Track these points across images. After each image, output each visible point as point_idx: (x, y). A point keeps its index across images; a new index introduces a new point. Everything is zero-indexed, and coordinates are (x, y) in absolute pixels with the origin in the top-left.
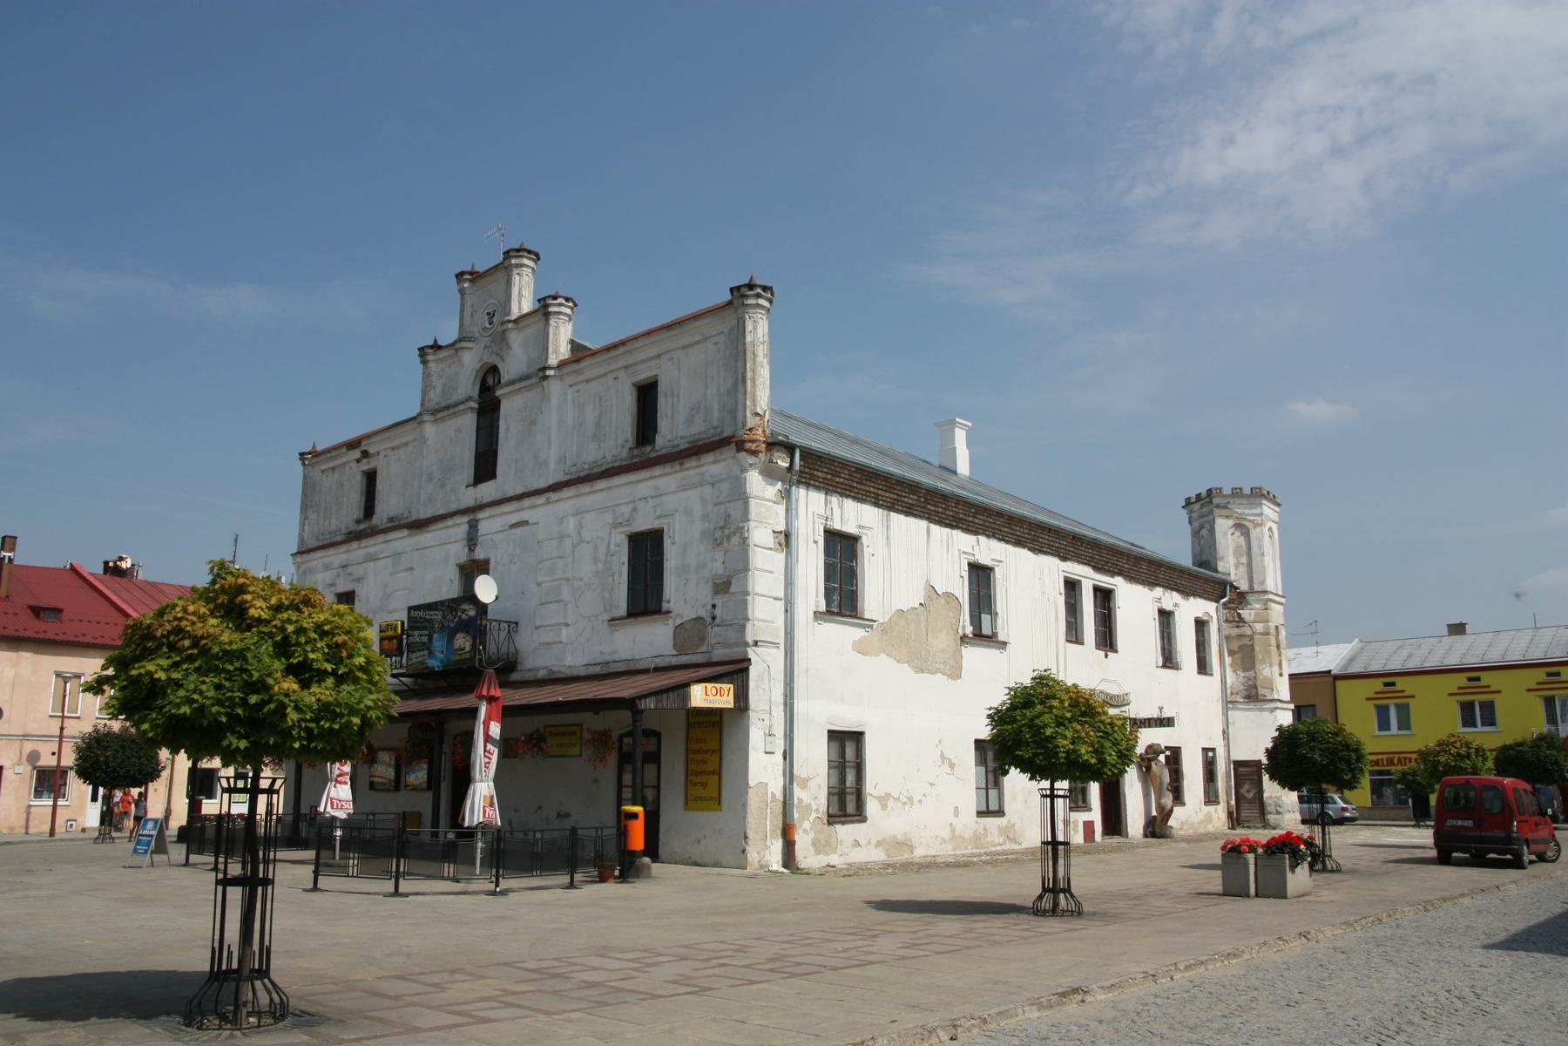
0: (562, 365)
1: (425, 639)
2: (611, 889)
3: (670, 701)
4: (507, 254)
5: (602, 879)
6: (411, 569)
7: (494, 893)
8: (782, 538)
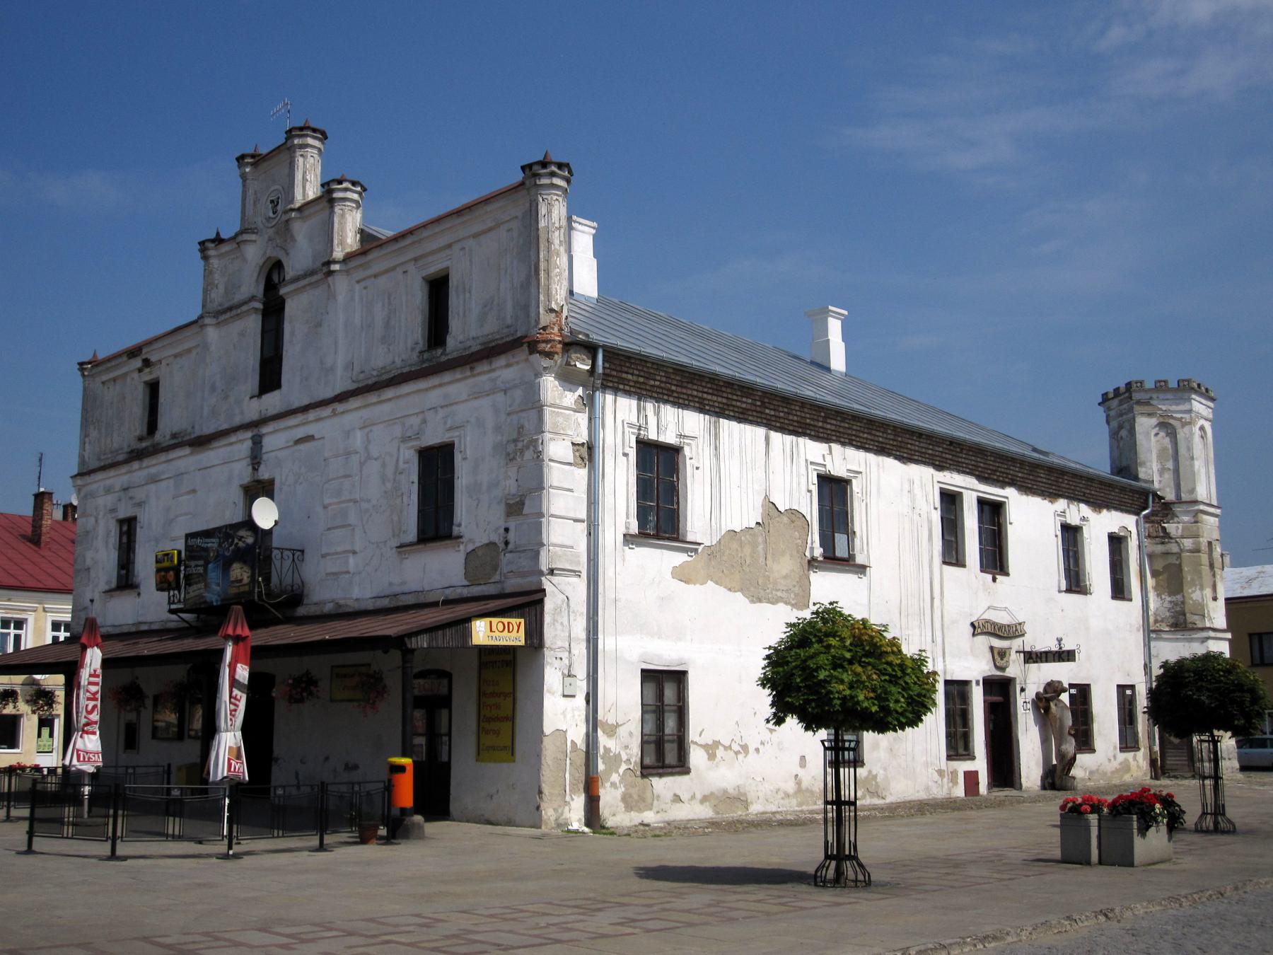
0: (349, 257)
1: (201, 570)
2: (372, 851)
3: (446, 639)
4: (290, 134)
5: (363, 840)
6: (194, 491)
7: (226, 857)
8: (584, 451)
